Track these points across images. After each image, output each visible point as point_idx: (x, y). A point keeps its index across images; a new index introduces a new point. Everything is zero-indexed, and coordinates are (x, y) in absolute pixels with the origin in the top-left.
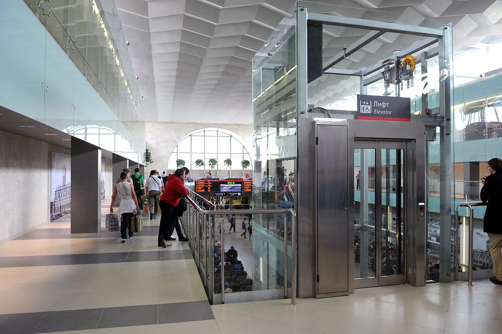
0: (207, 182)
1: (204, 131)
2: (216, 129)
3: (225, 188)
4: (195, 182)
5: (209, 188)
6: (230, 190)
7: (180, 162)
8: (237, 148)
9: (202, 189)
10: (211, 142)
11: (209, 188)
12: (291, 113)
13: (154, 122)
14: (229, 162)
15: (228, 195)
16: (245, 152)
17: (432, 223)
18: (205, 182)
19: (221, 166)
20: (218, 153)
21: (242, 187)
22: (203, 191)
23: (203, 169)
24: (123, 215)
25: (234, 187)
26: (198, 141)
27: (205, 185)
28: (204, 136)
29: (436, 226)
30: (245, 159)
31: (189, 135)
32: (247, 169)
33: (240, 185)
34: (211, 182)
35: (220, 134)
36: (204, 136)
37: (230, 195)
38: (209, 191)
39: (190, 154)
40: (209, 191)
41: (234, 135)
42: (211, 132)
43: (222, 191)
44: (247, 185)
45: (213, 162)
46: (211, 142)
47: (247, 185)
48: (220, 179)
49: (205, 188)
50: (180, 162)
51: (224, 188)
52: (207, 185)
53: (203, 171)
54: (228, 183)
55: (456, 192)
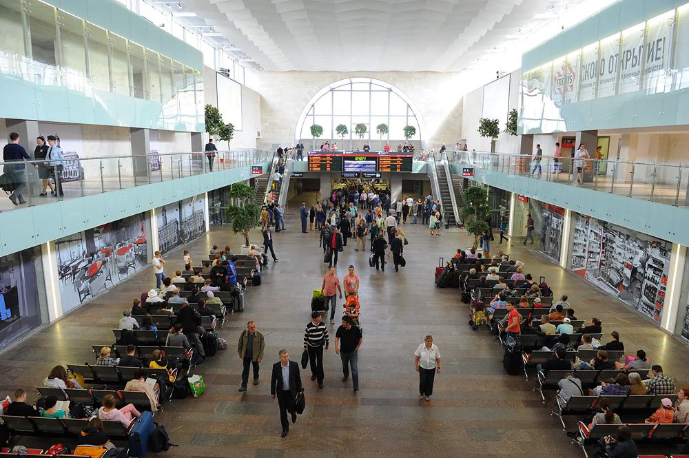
0: (326, 157)
1: (351, 83)
2: (368, 80)
3: (351, 166)
4: (309, 157)
5: (328, 165)
6: (358, 170)
7: (410, 130)
8: (398, 107)
9: (388, 167)
10: (361, 99)
11: (328, 165)
12: (15, 70)
13: (277, 72)
14: (383, 128)
15: (361, 176)
16: (410, 113)
17: (628, 244)
18: (392, 158)
19: (373, 135)
20: (389, 116)
21: (377, 166)
22: (389, 170)
23: (349, 138)
24: (208, 192)
25: (364, 165)
26: (342, 98)
27: (392, 161)
28: (370, 91)
29: (633, 249)
30: (316, 124)
31: (328, 88)
32: (411, 139)
33: (374, 162)
34: (401, 158)
35: (373, 88)
36: (351, 91)
37: (364, 176)
38: (328, 170)
39: (350, 117)
40: (328, 170)
41: (394, 89)
42: (361, 84)
43: (347, 170)
44: (384, 162)
45: (361, 128)
46: (361, 99)
47: (384, 162)
48: (344, 153)
49: (393, 167)
50: (410, 130)
51: (351, 166)
52: (396, 161)
53: (348, 141)
54: (356, 159)
55: (121, 174)
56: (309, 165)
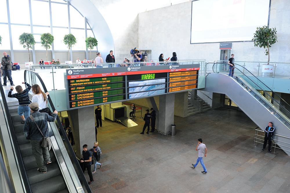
51: (137, 89)
56: (70, 99)
